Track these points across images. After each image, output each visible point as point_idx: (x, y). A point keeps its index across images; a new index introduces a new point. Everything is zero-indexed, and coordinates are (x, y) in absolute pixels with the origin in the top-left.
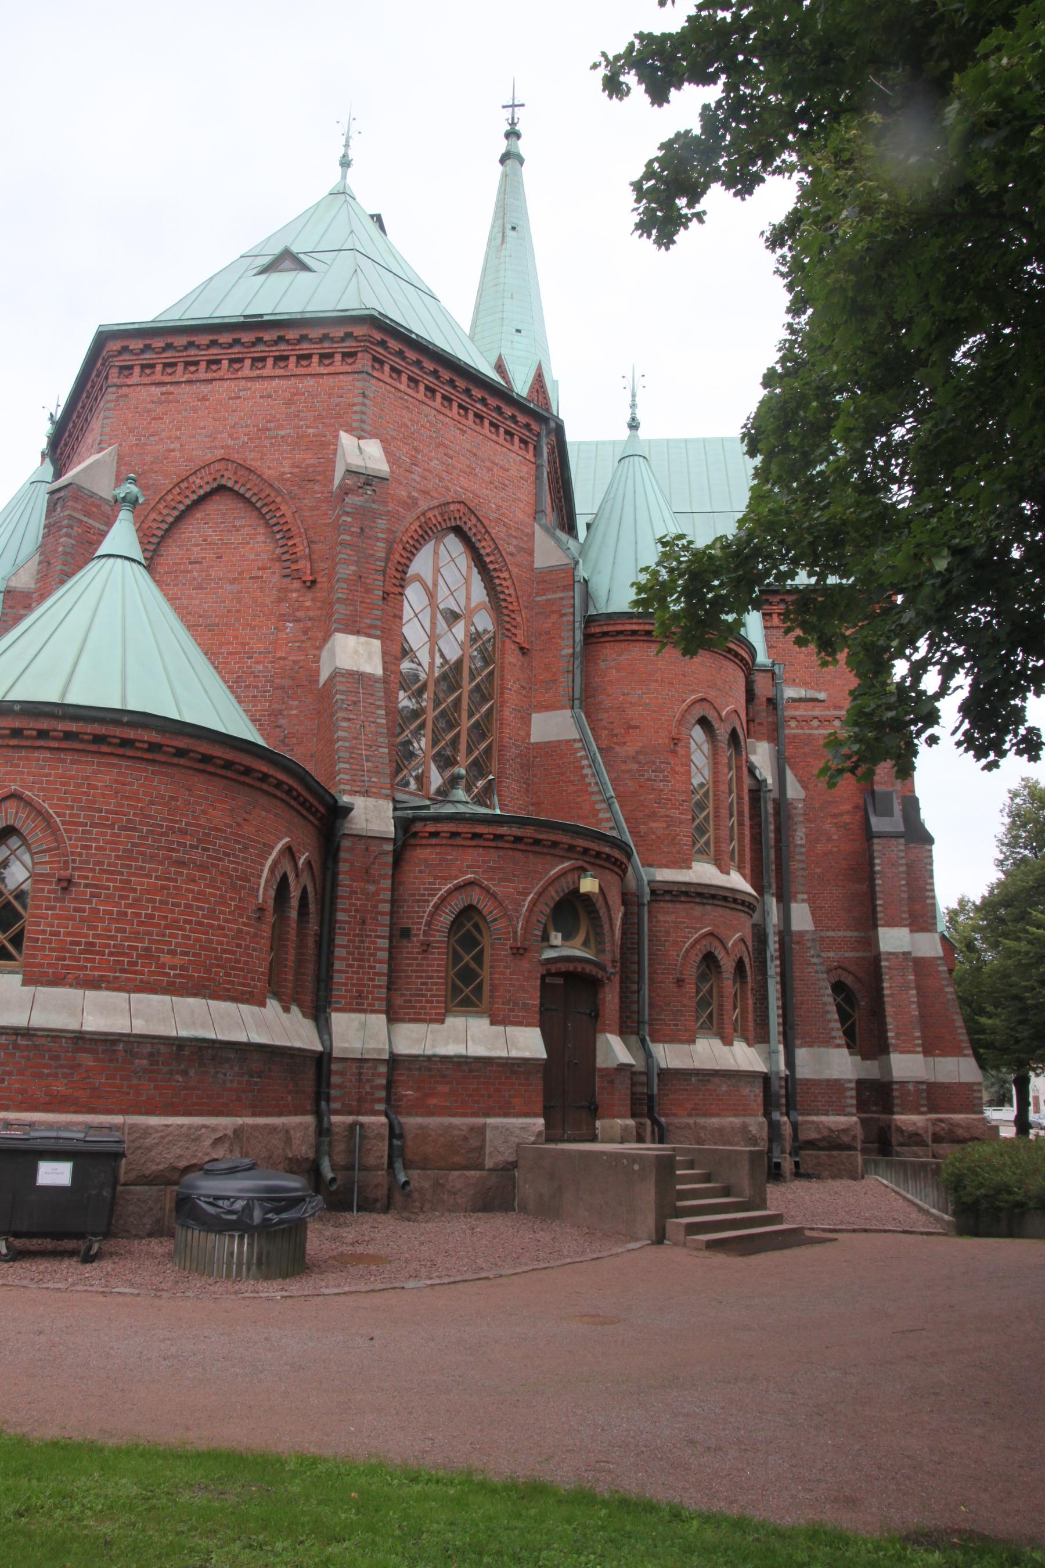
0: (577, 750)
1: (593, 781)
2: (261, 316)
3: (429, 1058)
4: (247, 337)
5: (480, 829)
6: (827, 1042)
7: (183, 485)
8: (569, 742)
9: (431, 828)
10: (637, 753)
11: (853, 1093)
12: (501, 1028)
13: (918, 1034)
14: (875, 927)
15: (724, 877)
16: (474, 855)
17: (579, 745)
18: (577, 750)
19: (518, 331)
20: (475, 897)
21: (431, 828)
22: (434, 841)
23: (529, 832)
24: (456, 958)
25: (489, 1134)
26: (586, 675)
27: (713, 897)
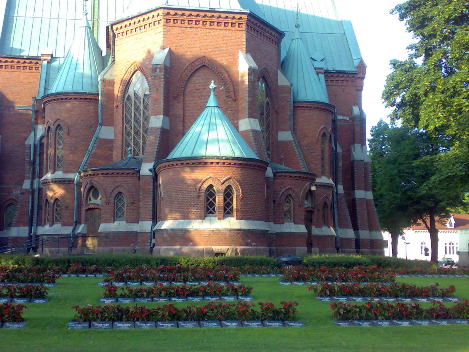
0: (293, 144)
1: (298, 153)
2: (214, 9)
3: (282, 233)
4: (209, 14)
5: (292, 175)
6: (347, 227)
7: (193, 64)
8: (290, 141)
9: (280, 174)
10: (307, 144)
11: (354, 242)
12: (297, 225)
13: (367, 224)
14: (353, 189)
15: (328, 180)
16: (290, 181)
17: (293, 142)
18: (293, 144)
20: (290, 192)
21: (280, 174)
22: (280, 178)
23: (302, 175)
24: (208, 199)
25: (296, 250)
26: (294, 119)
27: (327, 186)
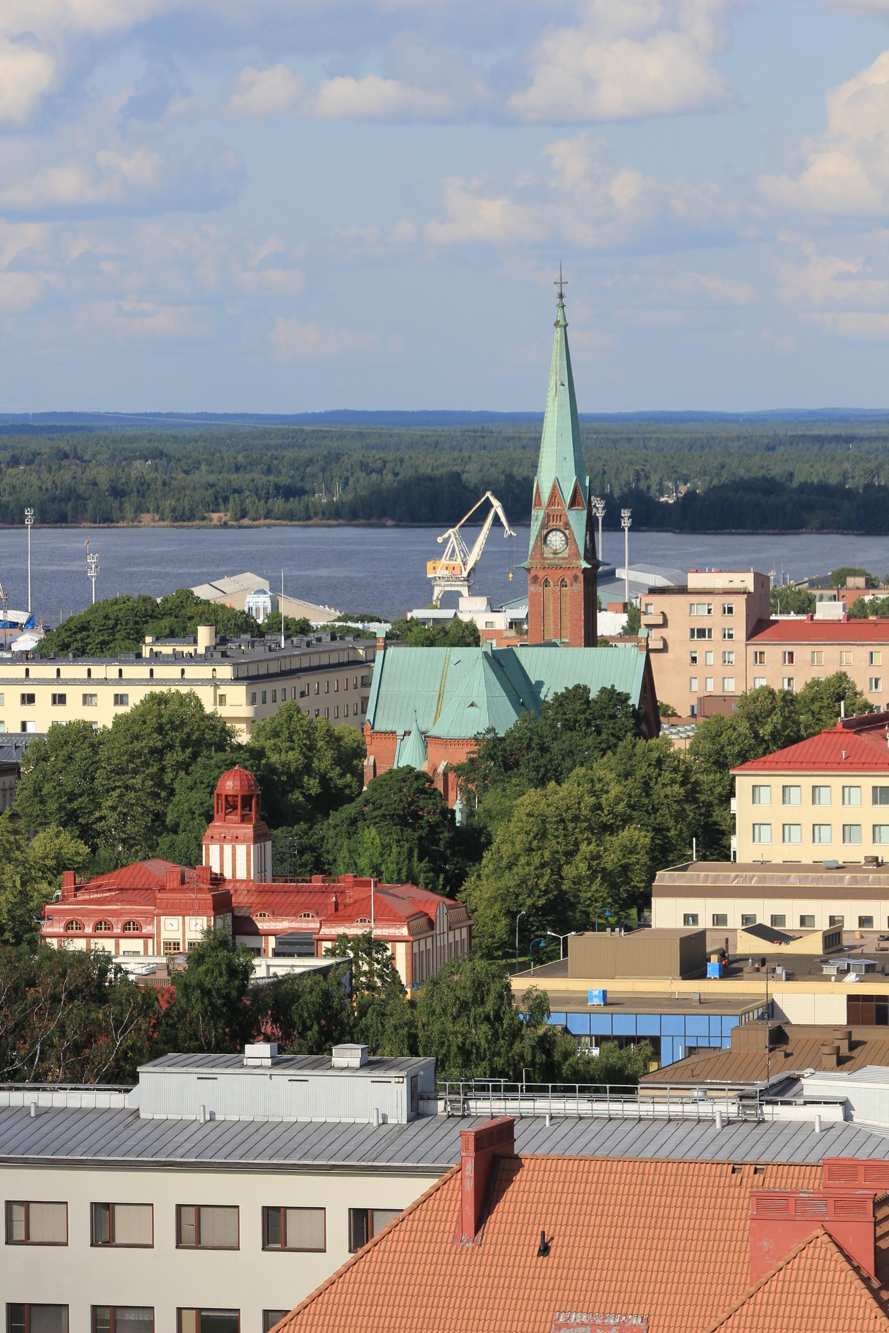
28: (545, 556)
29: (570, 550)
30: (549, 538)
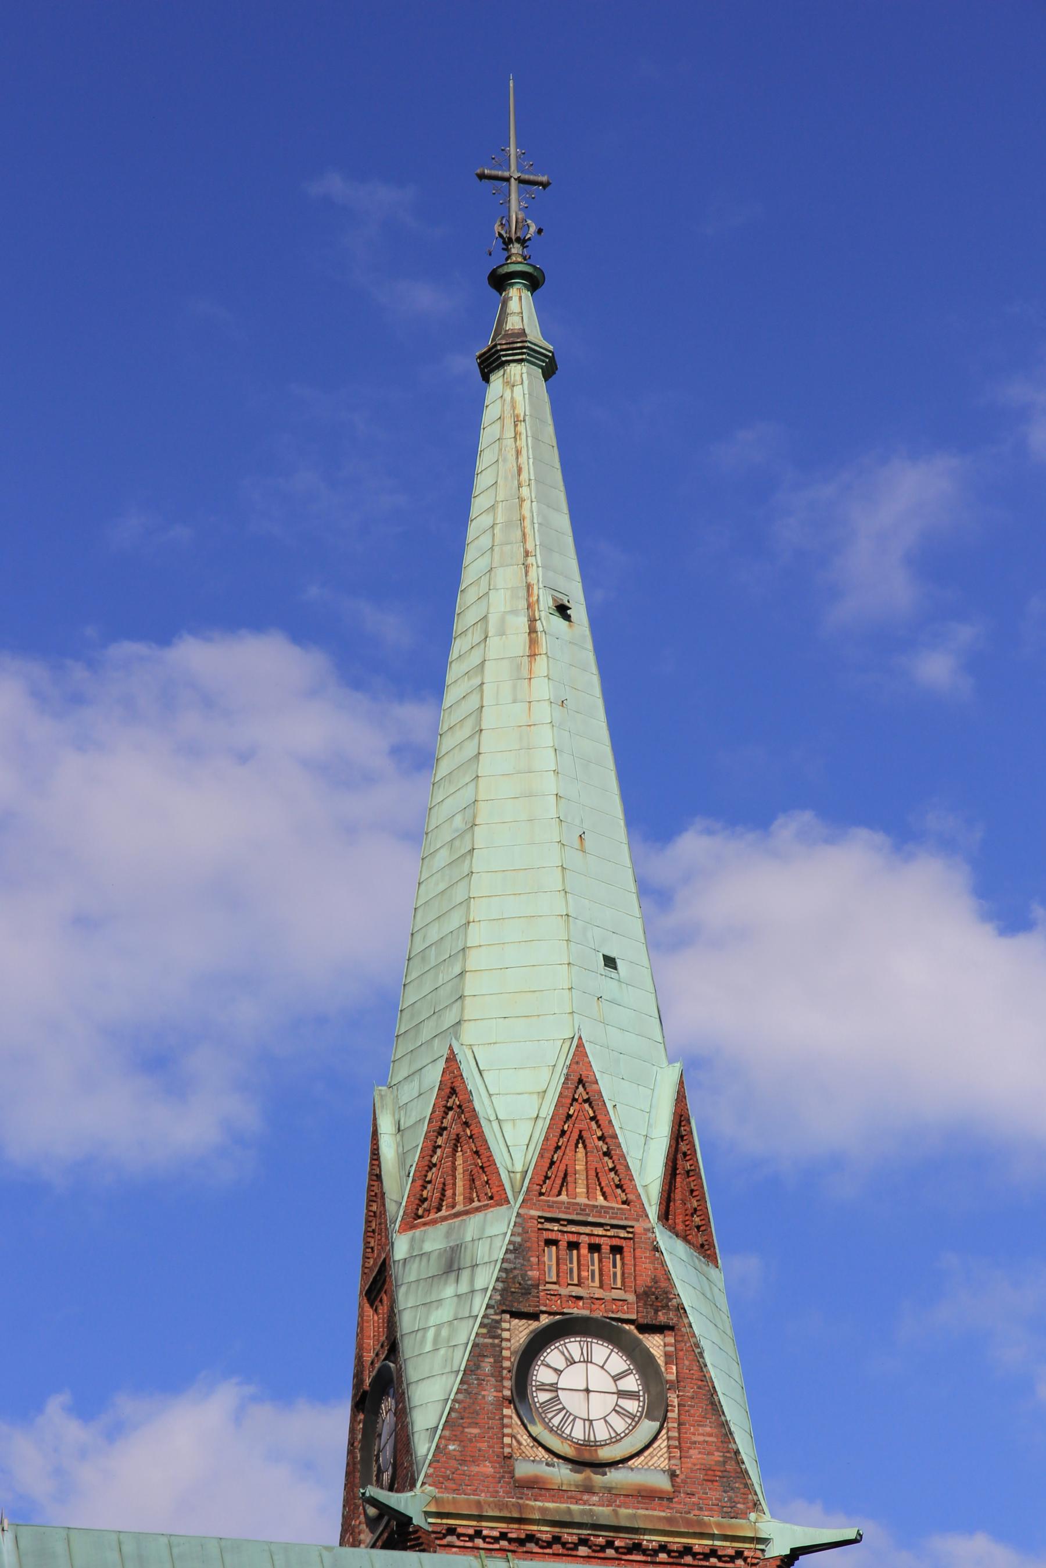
19: (610, 962)
28: (523, 1470)
29: (680, 1447)
30: (542, 1375)
